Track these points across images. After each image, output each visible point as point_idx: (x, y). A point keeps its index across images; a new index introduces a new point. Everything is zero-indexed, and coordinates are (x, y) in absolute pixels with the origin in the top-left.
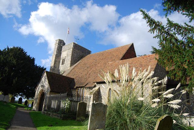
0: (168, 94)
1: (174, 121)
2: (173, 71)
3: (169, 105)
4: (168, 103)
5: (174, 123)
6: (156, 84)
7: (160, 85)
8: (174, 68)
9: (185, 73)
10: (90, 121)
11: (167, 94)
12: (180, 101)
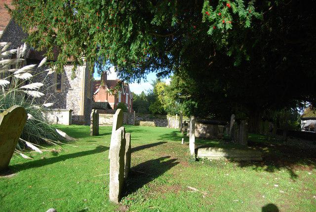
0: (23, 73)
1: (28, 114)
2: (35, 34)
3: (26, 92)
4: (22, 87)
5: (29, 118)
6: (4, 54)
7: (14, 56)
8: (37, 29)
9: (53, 41)
10: (127, 157)
11: (21, 73)
12: (41, 84)
